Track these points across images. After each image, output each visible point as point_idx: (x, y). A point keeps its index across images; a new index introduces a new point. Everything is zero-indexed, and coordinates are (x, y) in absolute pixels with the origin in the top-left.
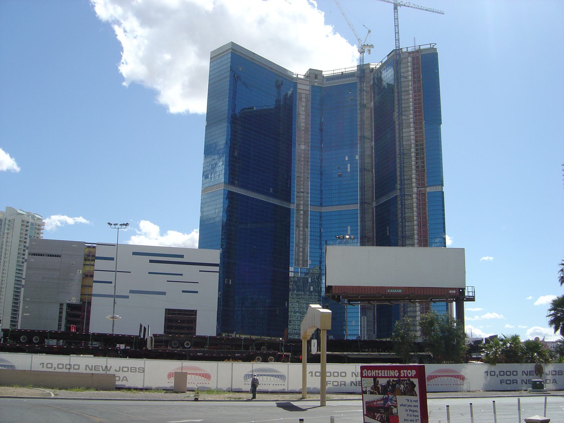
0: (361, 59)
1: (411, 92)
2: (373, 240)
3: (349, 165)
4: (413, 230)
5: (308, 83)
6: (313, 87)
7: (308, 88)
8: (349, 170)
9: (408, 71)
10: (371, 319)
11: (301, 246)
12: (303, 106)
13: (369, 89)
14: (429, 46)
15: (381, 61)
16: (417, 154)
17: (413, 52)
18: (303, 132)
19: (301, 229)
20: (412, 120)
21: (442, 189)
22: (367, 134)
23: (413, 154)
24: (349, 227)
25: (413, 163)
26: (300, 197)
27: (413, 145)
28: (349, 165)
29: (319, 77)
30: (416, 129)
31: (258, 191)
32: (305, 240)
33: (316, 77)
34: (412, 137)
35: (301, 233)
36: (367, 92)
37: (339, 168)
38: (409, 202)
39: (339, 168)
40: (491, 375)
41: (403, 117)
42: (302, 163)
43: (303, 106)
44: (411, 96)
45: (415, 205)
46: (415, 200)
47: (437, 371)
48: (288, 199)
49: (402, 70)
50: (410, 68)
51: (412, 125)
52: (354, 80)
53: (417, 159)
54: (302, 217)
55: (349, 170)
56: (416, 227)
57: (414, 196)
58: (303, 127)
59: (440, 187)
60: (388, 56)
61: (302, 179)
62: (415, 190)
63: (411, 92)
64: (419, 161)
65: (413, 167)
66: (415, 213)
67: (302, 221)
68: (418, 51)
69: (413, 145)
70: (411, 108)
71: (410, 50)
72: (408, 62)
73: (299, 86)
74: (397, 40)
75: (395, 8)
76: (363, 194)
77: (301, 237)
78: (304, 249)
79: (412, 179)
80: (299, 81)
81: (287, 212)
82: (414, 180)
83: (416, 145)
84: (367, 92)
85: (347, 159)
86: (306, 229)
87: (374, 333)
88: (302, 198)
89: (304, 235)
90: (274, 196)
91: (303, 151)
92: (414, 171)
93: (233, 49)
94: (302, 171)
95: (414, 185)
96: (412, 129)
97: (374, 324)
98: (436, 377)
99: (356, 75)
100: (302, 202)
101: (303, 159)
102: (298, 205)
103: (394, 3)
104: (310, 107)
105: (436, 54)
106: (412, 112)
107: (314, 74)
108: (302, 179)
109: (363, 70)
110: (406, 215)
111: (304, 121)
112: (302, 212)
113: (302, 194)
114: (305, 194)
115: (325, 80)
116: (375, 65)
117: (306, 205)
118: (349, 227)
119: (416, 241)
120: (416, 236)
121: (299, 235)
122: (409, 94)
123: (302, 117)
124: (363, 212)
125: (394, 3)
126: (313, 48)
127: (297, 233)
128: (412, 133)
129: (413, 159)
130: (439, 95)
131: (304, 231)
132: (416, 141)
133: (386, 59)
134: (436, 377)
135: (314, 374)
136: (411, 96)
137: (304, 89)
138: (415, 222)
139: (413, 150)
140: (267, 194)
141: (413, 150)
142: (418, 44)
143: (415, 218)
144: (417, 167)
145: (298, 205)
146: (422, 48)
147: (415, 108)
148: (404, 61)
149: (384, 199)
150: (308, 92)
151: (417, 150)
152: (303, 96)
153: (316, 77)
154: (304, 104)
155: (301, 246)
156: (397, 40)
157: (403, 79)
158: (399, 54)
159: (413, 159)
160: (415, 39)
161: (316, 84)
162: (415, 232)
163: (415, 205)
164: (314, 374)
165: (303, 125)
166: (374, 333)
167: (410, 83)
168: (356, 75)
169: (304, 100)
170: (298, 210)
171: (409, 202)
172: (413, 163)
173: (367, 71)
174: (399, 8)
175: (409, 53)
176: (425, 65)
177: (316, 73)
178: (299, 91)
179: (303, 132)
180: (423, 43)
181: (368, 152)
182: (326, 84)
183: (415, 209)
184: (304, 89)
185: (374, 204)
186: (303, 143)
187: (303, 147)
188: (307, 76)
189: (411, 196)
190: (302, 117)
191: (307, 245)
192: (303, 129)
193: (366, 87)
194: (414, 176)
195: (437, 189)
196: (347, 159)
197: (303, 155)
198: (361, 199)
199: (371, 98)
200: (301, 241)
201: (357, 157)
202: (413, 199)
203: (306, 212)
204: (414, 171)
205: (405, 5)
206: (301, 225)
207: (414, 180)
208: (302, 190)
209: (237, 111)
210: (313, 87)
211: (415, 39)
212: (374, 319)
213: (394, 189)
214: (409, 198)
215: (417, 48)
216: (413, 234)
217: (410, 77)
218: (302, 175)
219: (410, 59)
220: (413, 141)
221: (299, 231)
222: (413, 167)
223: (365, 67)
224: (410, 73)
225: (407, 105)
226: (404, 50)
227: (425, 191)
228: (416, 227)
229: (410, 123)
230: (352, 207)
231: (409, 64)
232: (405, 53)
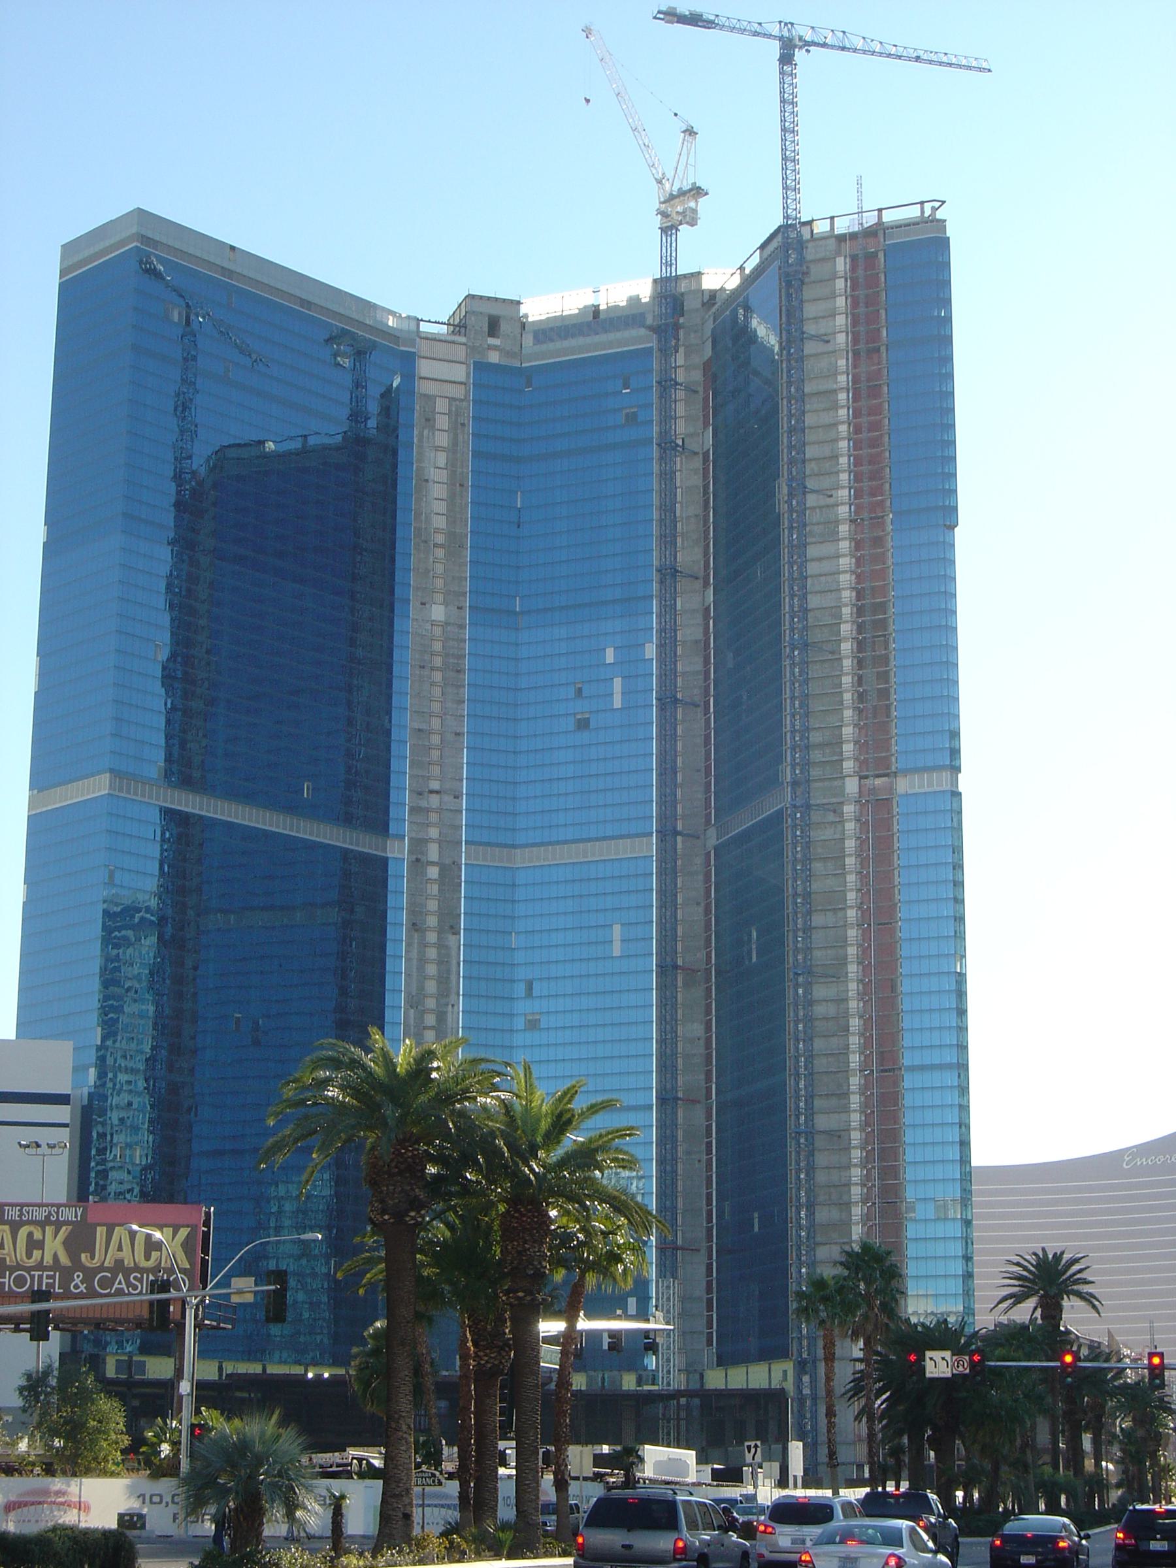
0: (668, 261)
1: (842, 396)
2: (708, 980)
3: (618, 683)
4: (844, 943)
5: (460, 353)
6: (481, 367)
7: (459, 373)
8: (617, 703)
9: (833, 315)
10: (700, 1291)
11: (431, 1003)
12: (437, 449)
13: (697, 376)
14: (914, 212)
15: (742, 268)
16: (861, 645)
17: (853, 236)
18: (440, 553)
19: (432, 937)
20: (843, 511)
21: (955, 782)
22: (689, 556)
23: (846, 647)
24: (617, 929)
25: (847, 680)
26: (428, 810)
27: (846, 611)
28: (618, 683)
29: (504, 327)
30: (858, 545)
31: (248, 797)
32: (445, 981)
33: (494, 326)
34: (842, 577)
35: (432, 953)
36: (691, 390)
37: (579, 692)
38: (828, 833)
39: (579, 692)
40: (151, 1502)
41: (811, 500)
42: (437, 676)
43: (437, 449)
44: (843, 412)
45: (850, 844)
46: (850, 826)
47: (28, 1493)
48: (380, 825)
49: (810, 310)
50: (841, 302)
51: (844, 529)
52: (640, 339)
53: (860, 663)
54: (434, 889)
55: (617, 703)
56: (852, 933)
57: (849, 809)
58: (437, 530)
59: (946, 775)
60: (762, 247)
61: (435, 739)
62: (852, 786)
63: (842, 396)
64: (869, 672)
65: (847, 697)
66: (851, 878)
67: (433, 905)
68: (877, 231)
69: (846, 611)
70: (843, 460)
71: (842, 227)
72: (834, 277)
73: (425, 368)
74: (789, 188)
75: (786, 59)
76: (667, 801)
77: (431, 969)
78: (441, 1017)
79: (841, 743)
80: (424, 348)
81: (375, 872)
82: (848, 748)
83: (860, 611)
84: (691, 390)
85: (610, 656)
86: (452, 938)
87: (709, 1343)
88: (434, 817)
89: (444, 962)
90: (311, 811)
91: (438, 631)
92: (848, 713)
93: (145, 239)
94: (436, 707)
95: (848, 766)
96: (844, 546)
97: (710, 1309)
98: (26, 1504)
99: (649, 321)
100: (434, 833)
101: (438, 661)
102: (419, 844)
103: (781, 38)
104: (468, 444)
105: (943, 244)
106: (844, 477)
107: (486, 319)
108: (435, 739)
109: (674, 296)
110: (816, 886)
111: (442, 507)
112: (433, 872)
113: (434, 801)
114: (448, 798)
115: (528, 341)
116: (720, 277)
117: (450, 843)
118: (617, 929)
119: (853, 986)
120: (853, 969)
121: (423, 961)
122: (835, 407)
123: (438, 491)
124: (668, 869)
125: (781, 38)
126: (489, 206)
127: (414, 954)
128: (845, 562)
129: (847, 663)
130: (949, 411)
131: (441, 946)
132: (860, 595)
133: (756, 260)
134: (26, 1504)
135: (147, 1498)
136: (843, 412)
137: (443, 378)
138: (852, 914)
139: (846, 629)
140: (292, 807)
141: (846, 629)
142: (870, 204)
143: (851, 896)
144: (861, 697)
145: (419, 844)
146: (888, 217)
147: (858, 462)
148: (816, 271)
149: (744, 821)
150: (459, 392)
151: (860, 628)
152: (442, 405)
153: (494, 326)
154: (442, 439)
155: (431, 1003)
156: (789, 188)
157: (810, 348)
158: (801, 244)
159: (847, 663)
160: (859, 184)
161: (494, 358)
162: (852, 951)
163: (850, 844)
164: (147, 1498)
165: (440, 522)
166: (709, 1343)
167: (842, 363)
168: (649, 321)
169: (442, 422)
170: (418, 864)
171: (828, 833)
172: (847, 680)
173: (691, 304)
174: (799, 55)
175: (841, 238)
176: (895, 280)
177: (495, 310)
178: (424, 387)
179: (440, 553)
180: (892, 196)
181: (689, 631)
182: (534, 355)
183: (850, 861)
184: (443, 378)
185: (712, 839)
186: (439, 598)
187: (438, 612)
188: (459, 326)
189: (837, 809)
190: (438, 491)
191: (453, 997)
192: (440, 539)
193: (687, 367)
194: (848, 731)
195: (940, 781)
196: (610, 656)
197: (437, 646)
198: (662, 817)
199: (706, 417)
200: (431, 987)
201: (651, 651)
202: (842, 822)
203: (449, 872)
204: (848, 713)
205: (824, 45)
206: (432, 921)
207: (848, 748)
208: (435, 785)
209: (199, 463)
210: (481, 367)
211: (859, 184)
212: (709, 1290)
213: (773, 781)
214: (831, 817)
215: (870, 220)
216: (843, 962)
217: (841, 339)
218: (436, 723)
219: (841, 264)
220: (847, 595)
221: (424, 945)
222: (847, 697)
223: (683, 287)
224: (841, 320)
225: (826, 451)
226: (821, 227)
227: (891, 789)
228: (852, 933)
229: (837, 522)
230: (624, 849)
231: (840, 284)
232: (824, 238)
